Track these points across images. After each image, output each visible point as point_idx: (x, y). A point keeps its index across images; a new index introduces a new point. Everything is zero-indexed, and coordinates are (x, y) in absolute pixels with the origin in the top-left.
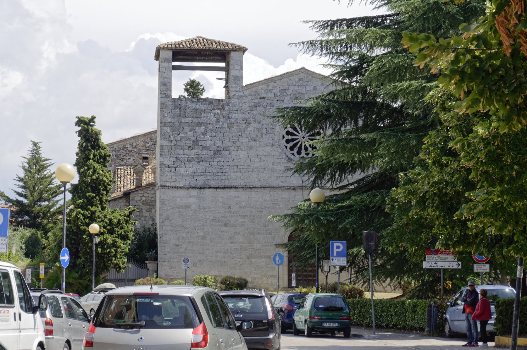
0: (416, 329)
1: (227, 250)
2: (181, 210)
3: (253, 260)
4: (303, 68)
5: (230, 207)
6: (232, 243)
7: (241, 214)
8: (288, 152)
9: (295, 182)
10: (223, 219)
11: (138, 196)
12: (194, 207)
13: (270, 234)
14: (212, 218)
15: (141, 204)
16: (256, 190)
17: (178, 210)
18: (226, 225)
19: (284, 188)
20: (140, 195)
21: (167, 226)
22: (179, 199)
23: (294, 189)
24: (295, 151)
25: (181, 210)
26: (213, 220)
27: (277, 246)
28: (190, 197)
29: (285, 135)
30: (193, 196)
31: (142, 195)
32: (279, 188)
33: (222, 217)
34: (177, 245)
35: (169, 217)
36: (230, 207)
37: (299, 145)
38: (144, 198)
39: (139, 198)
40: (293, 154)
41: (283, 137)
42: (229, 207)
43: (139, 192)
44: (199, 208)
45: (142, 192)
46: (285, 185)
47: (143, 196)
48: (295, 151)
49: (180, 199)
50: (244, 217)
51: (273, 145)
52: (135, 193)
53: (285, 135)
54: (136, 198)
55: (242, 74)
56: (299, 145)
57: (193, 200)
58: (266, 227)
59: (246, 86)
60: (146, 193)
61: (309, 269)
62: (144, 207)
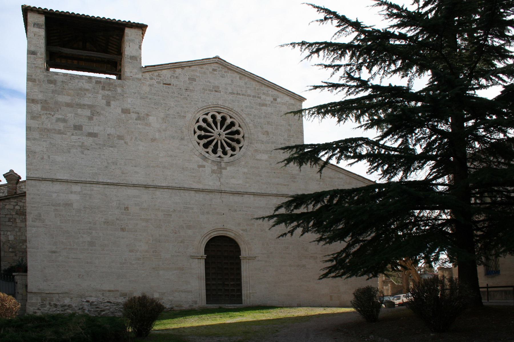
0: (182, 291)
1: (125, 260)
2: (58, 208)
3: (161, 272)
4: (217, 58)
5: (127, 208)
6: (131, 251)
7: (143, 217)
8: (203, 150)
9: (211, 183)
10: (118, 222)
11: (10, 204)
12: (75, 206)
13: (181, 242)
14: (103, 220)
15: (14, 213)
16: (162, 190)
17: (53, 207)
18: (123, 230)
19: (197, 191)
20: (12, 203)
21: (38, 227)
22: (54, 195)
23: (211, 191)
24: (210, 149)
25: (58, 208)
26: (105, 222)
27: (193, 257)
28: (71, 192)
29: (197, 130)
30: (75, 192)
31: (15, 204)
32: (191, 189)
33: (117, 219)
34: (54, 252)
35: (40, 216)
36: (127, 208)
37: (229, 131)
38: (17, 208)
39: (12, 207)
40: (208, 152)
41: (195, 132)
42: (127, 208)
43: (12, 200)
44: (84, 208)
45: (15, 200)
46: (200, 186)
47: (17, 205)
48: (210, 149)
49: (56, 194)
50: (147, 220)
51: (182, 139)
52: (7, 201)
53: (197, 130)
54: (7, 207)
55: (141, 54)
56: (229, 131)
57: (74, 197)
58: (176, 233)
59: (146, 67)
60: (21, 201)
61: (232, 283)
62: (18, 216)
